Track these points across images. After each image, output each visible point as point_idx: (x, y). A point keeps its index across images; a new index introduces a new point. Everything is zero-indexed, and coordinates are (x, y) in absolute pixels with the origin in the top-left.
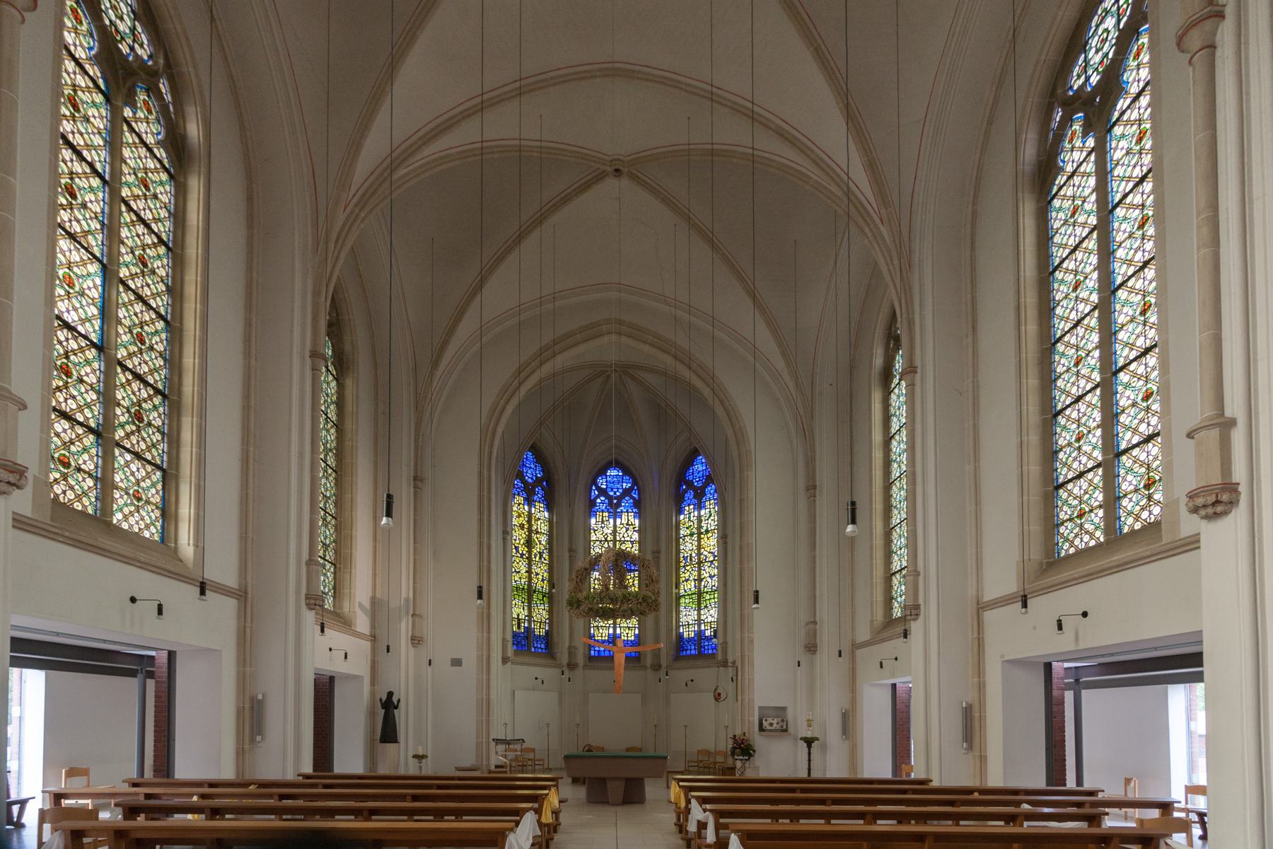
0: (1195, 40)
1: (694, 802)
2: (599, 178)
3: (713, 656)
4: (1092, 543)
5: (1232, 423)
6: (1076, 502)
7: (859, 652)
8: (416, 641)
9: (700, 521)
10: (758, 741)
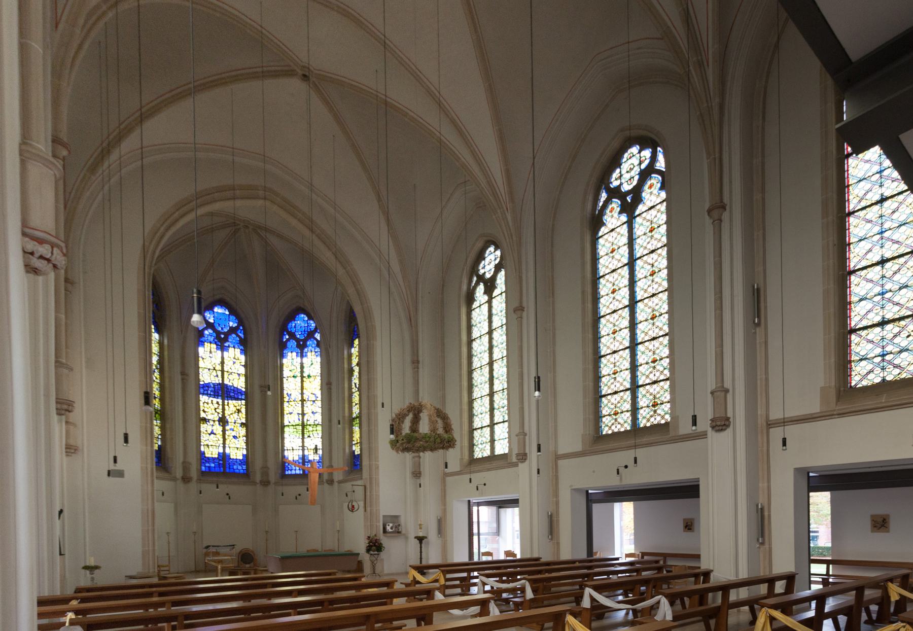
0: (715, 214)
2: (289, 73)
4: (622, 430)
5: (727, 391)
6: (613, 406)
7: (448, 479)
8: (71, 449)
9: (302, 367)
10: (385, 541)
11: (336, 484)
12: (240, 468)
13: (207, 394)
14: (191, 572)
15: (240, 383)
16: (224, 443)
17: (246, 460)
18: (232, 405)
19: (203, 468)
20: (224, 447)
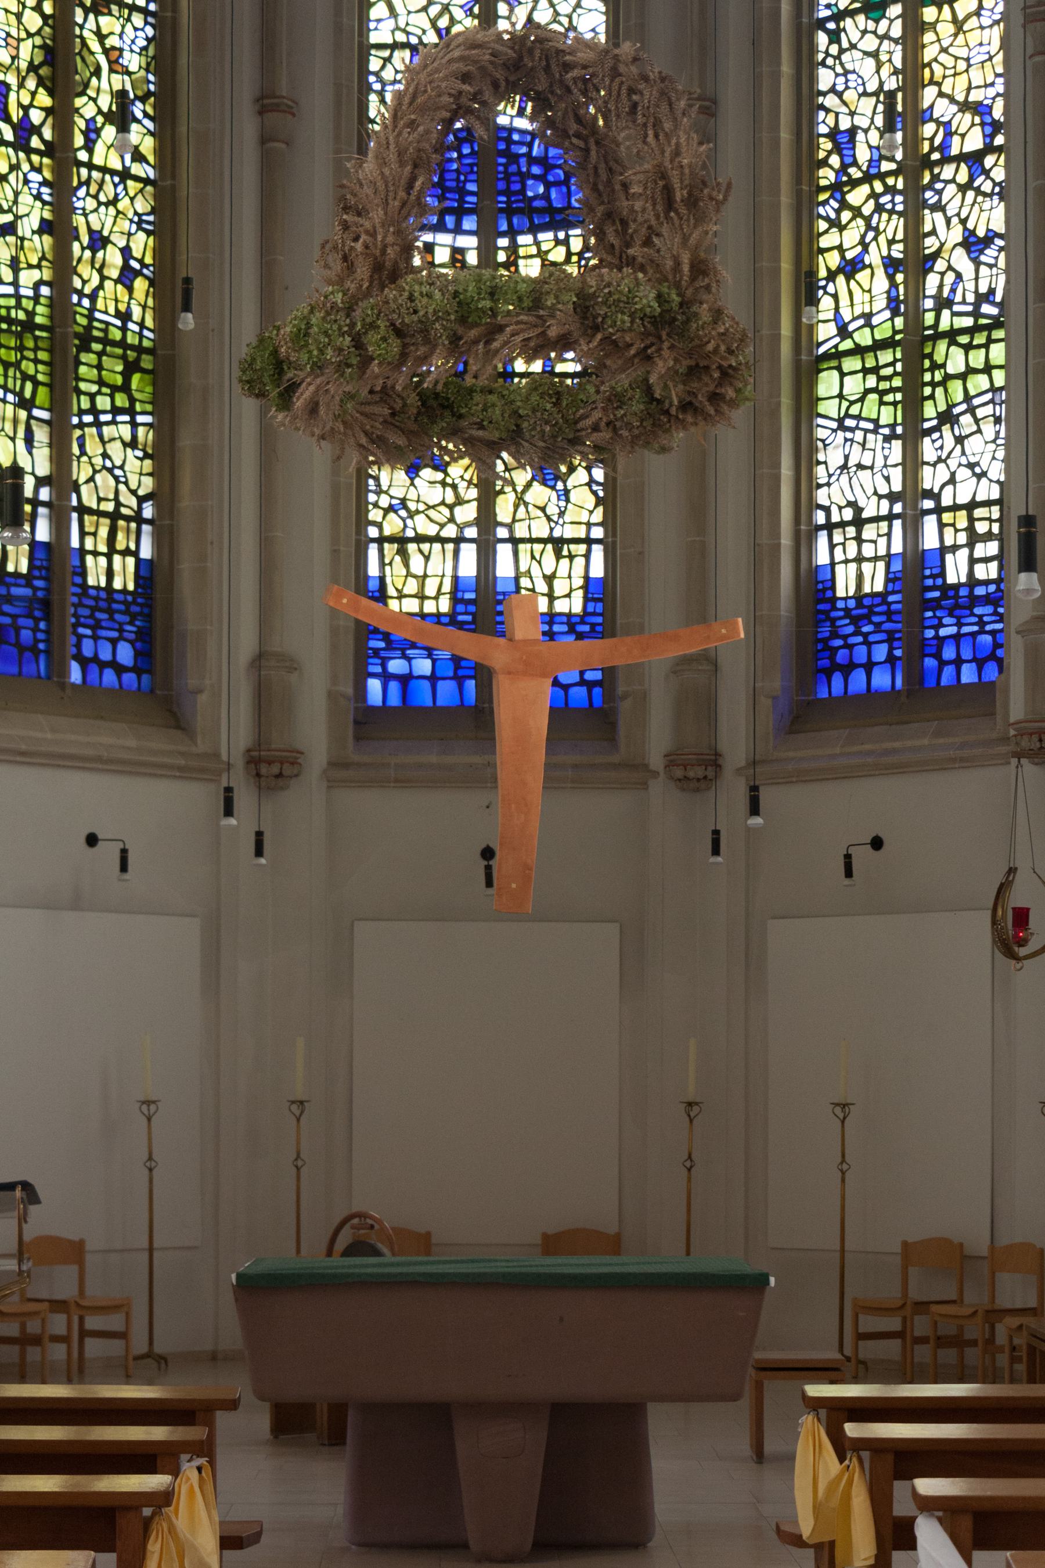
1: (930, 1534)
3: (985, 694)
19: (374, 686)
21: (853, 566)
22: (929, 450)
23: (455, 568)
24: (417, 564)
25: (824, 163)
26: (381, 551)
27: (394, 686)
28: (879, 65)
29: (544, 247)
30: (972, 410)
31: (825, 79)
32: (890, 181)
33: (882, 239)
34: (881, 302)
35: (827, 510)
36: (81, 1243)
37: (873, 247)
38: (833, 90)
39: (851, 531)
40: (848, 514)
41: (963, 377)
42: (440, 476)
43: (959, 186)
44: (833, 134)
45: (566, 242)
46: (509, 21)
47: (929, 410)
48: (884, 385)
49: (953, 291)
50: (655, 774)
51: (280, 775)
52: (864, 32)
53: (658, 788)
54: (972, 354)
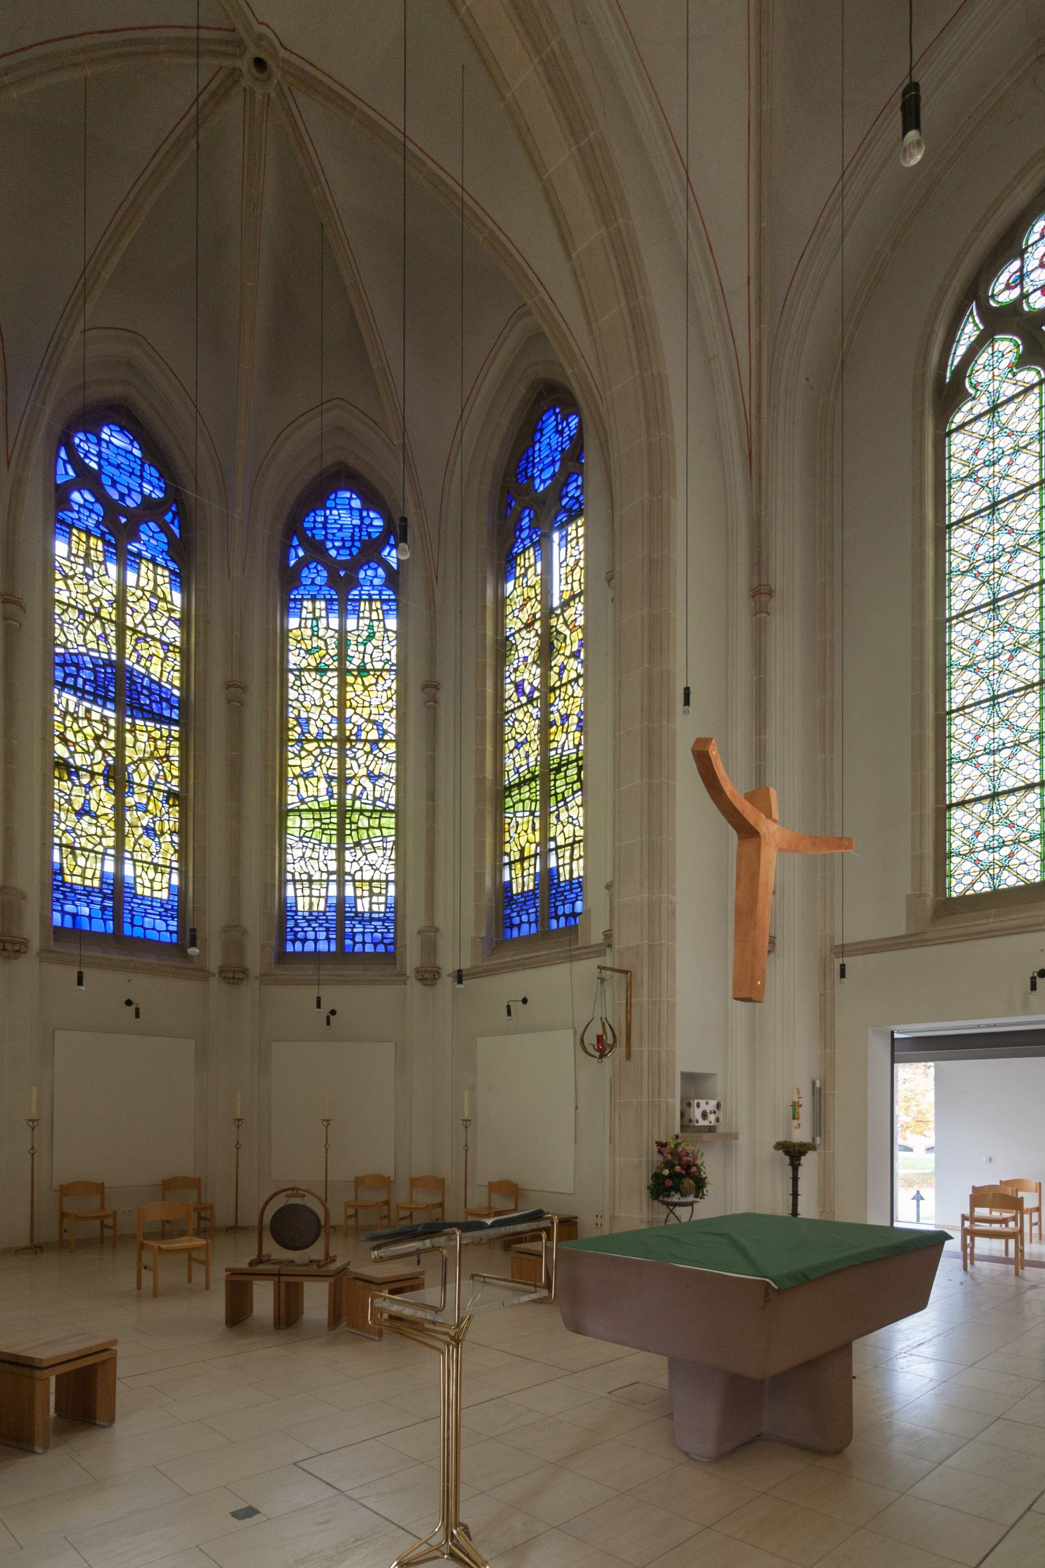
9: (343, 643)
11: (447, 983)
12: (161, 925)
13: (75, 689)
14: (17, 1251)
15: (163, 669)
16: (119, 846)
17: (181, 906)
18: (144, 738)
19: (57, 916)
20: (119, 861)
21: (307, 899)
22: (348, 856)
23: (102, 866)
24: (81, 861)
25: (292, 729)
26: (61, 851)
27: (68, 918)
28: (323, 695)
29: (150, 729)
30: (371, 843)
31: (292, 694)
32: (329, 744)
33: (323, 766)
34: (323, 792)
35: (293, 874)
36: (103, 1184)
37: (318, 769)
38: (297, 700)
39: (306, 884)
40: (305, 877)
41: (367, 829)
42: (94, 821)
43: (366, 752)
44: (297, 718)
45: (160, 730)
46: (996, 367)
47: (348, 840)
48: (323, 826)
49: (362, 793)
50: (213, 975)
51: (18, 951)
52: (315, 679)
53: (215, 982)
54: (371, 821)
